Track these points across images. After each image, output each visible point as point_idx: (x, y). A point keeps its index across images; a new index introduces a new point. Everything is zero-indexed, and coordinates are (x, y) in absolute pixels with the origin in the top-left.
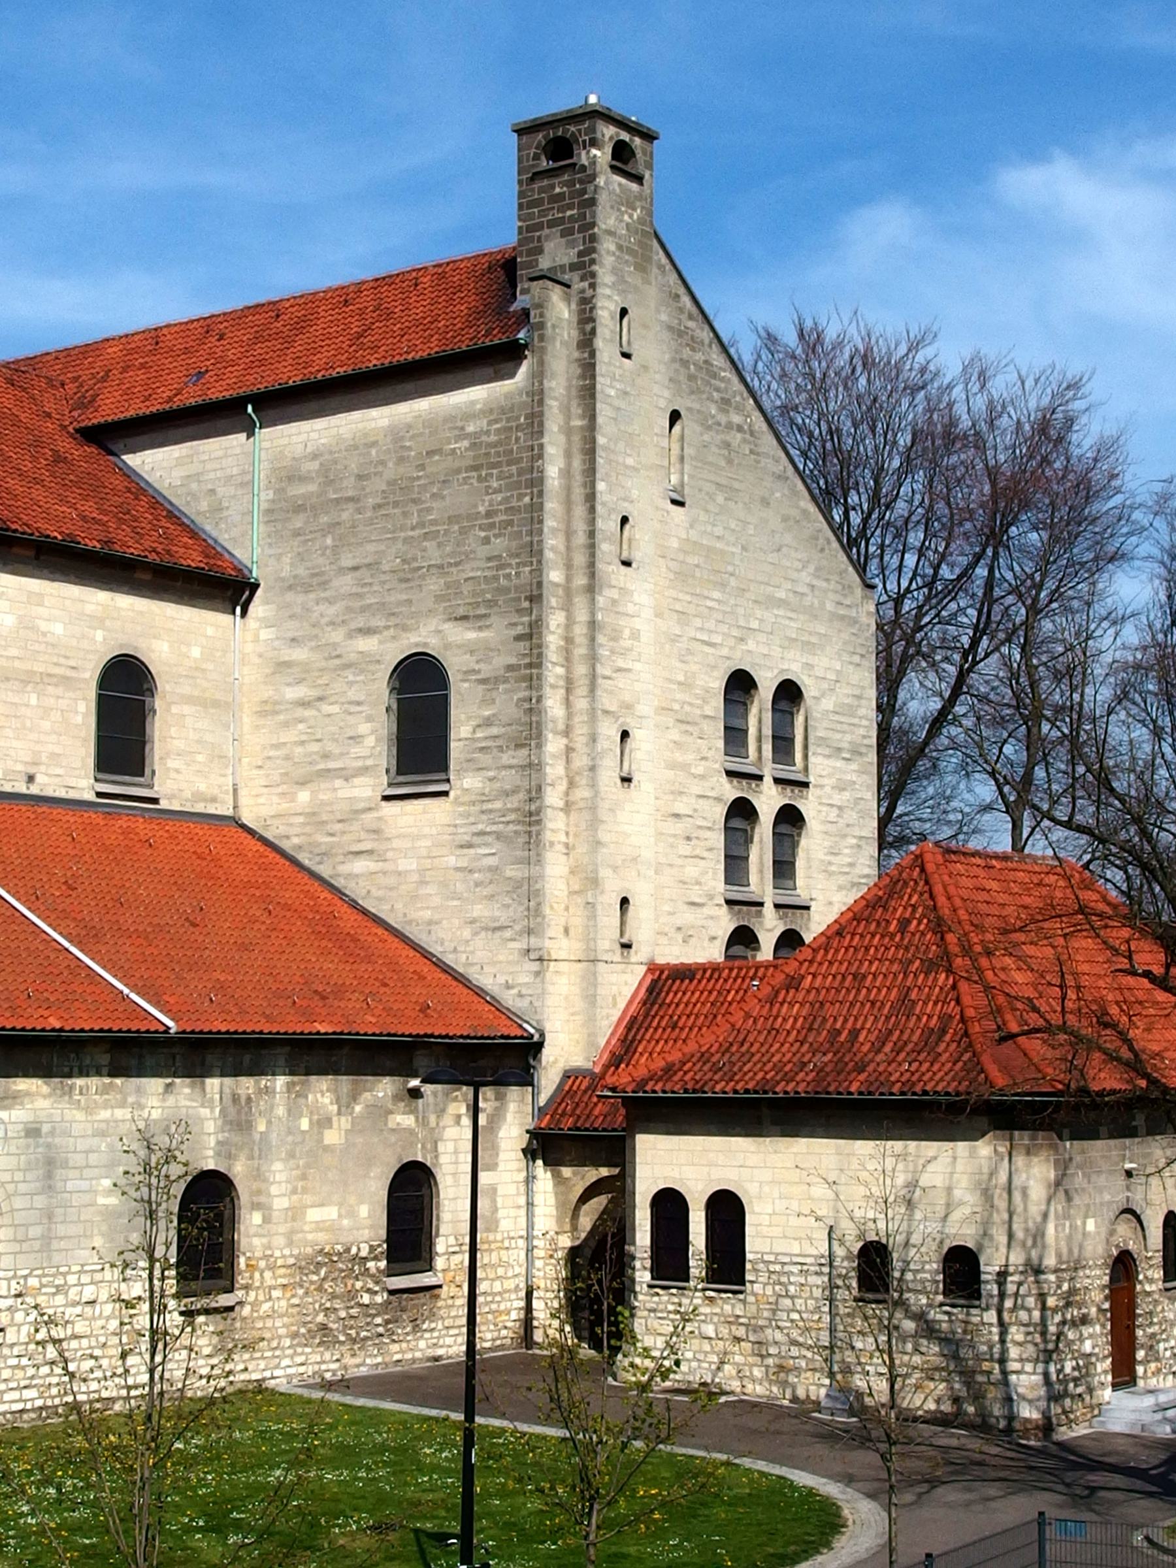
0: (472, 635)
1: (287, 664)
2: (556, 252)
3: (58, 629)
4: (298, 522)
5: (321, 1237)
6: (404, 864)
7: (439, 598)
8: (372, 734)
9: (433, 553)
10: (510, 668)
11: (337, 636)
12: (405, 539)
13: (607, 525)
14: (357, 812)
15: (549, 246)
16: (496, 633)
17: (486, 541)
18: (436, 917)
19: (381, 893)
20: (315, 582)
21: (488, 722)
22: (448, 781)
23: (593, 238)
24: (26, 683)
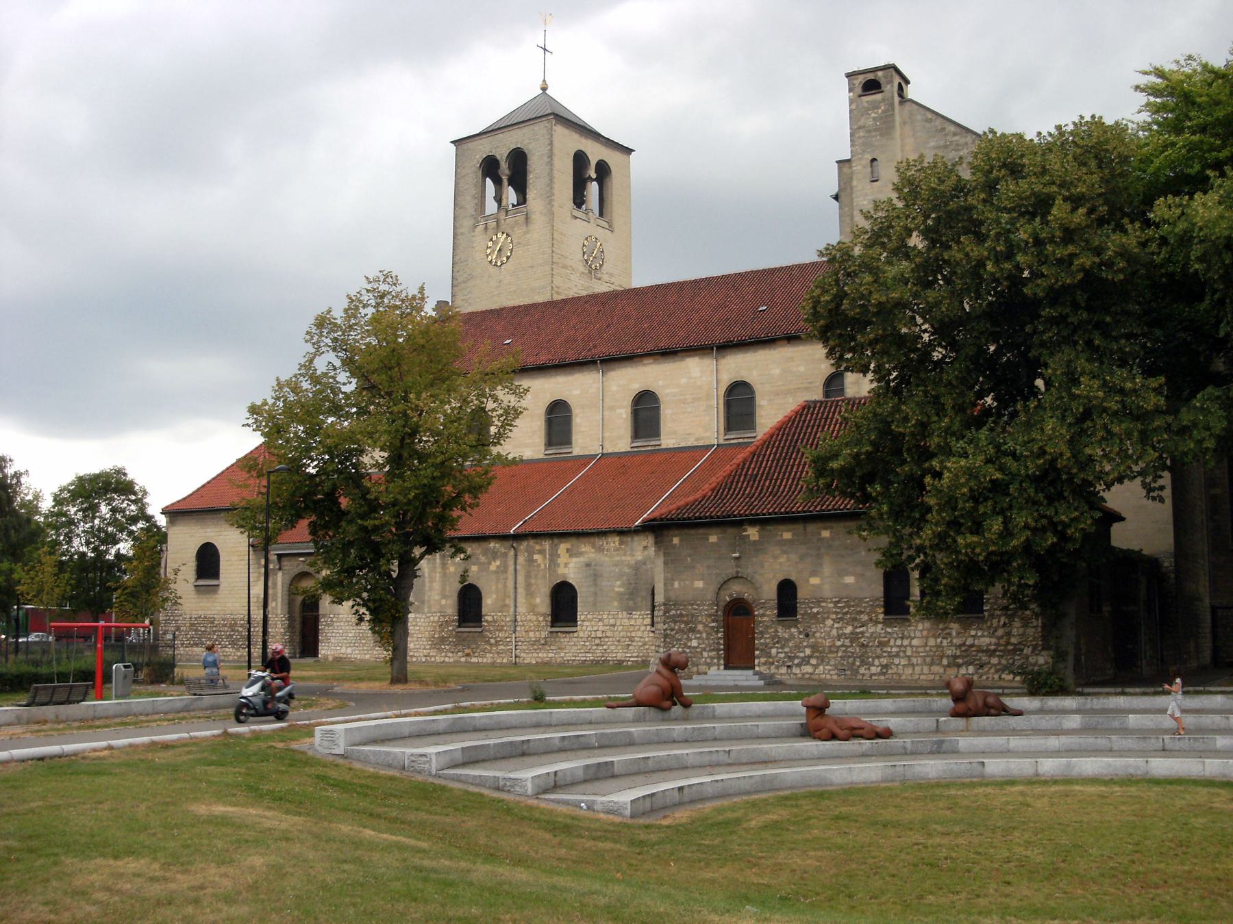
3: (802, 369)
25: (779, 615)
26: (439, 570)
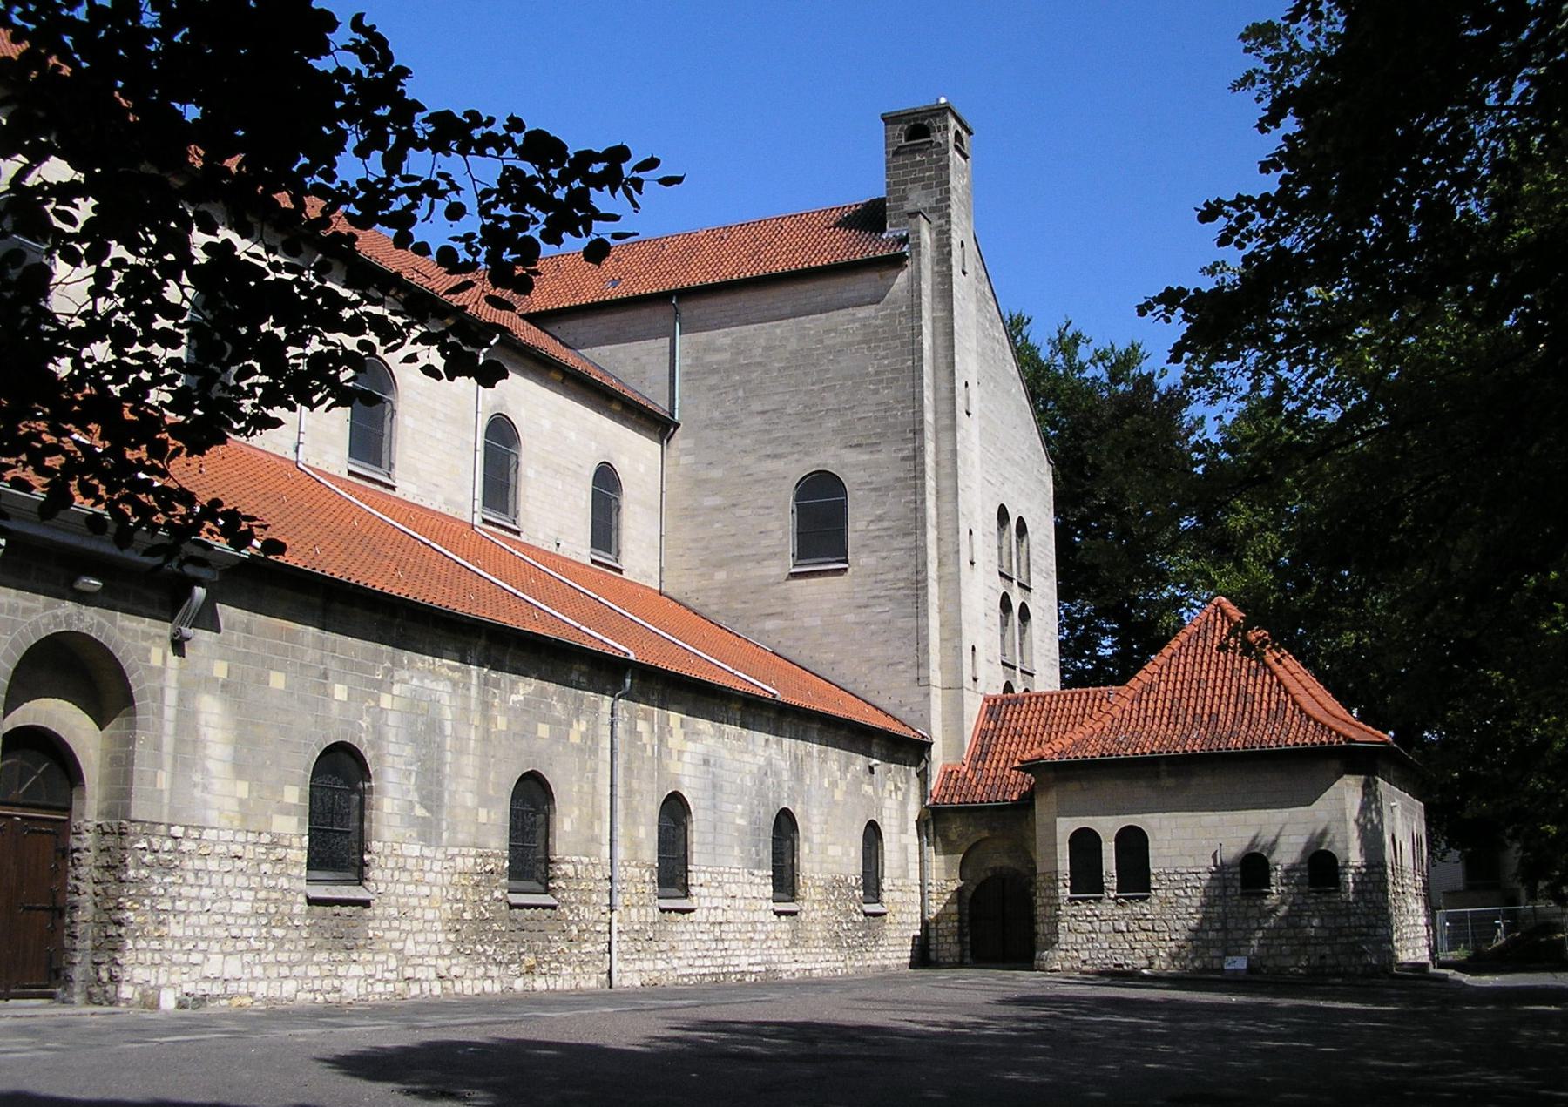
0: (865, 457)
1: (706, 481)
2: (918, 198)
4: (713, 380)
5: (835, 868)
6: (808, 621)
7: (836, 432)
8: (781, 529)
9: (831, 401)
10: (897, 480)
11: (748, 460)
12: (806, 392)
13: (960, 385)
14: (767, 585)
15: (913, 196)
16: (888, 457)
17: (876, 392)
18: (839, 658)
19: (790, 643)
20: (729, 423)
21: (880, 518)
22: (846, 561)
23: (948, 190)
24: (557, 472)
25: (912, 966)
26: (476, 719)
